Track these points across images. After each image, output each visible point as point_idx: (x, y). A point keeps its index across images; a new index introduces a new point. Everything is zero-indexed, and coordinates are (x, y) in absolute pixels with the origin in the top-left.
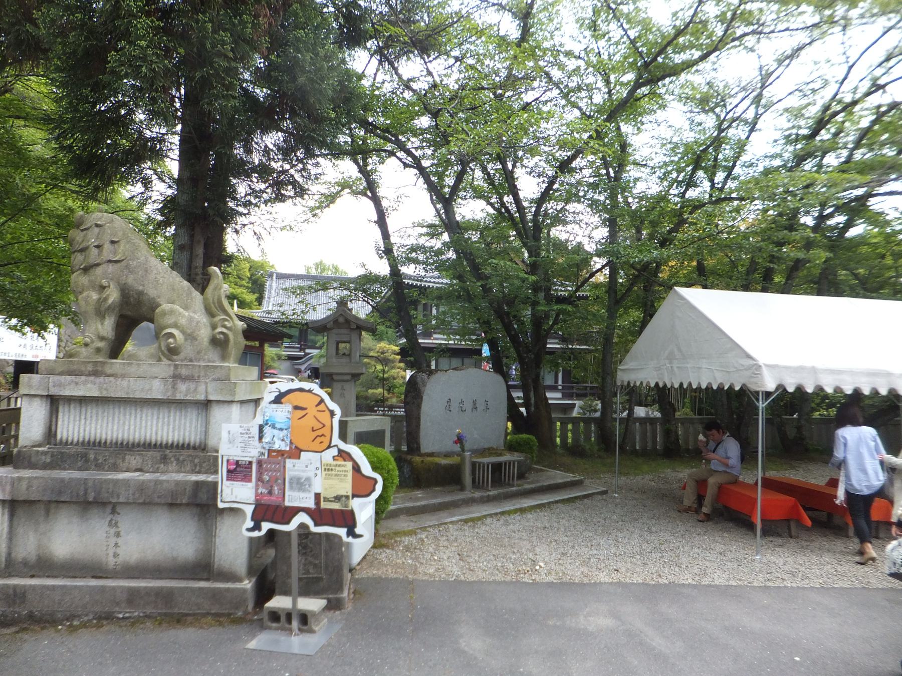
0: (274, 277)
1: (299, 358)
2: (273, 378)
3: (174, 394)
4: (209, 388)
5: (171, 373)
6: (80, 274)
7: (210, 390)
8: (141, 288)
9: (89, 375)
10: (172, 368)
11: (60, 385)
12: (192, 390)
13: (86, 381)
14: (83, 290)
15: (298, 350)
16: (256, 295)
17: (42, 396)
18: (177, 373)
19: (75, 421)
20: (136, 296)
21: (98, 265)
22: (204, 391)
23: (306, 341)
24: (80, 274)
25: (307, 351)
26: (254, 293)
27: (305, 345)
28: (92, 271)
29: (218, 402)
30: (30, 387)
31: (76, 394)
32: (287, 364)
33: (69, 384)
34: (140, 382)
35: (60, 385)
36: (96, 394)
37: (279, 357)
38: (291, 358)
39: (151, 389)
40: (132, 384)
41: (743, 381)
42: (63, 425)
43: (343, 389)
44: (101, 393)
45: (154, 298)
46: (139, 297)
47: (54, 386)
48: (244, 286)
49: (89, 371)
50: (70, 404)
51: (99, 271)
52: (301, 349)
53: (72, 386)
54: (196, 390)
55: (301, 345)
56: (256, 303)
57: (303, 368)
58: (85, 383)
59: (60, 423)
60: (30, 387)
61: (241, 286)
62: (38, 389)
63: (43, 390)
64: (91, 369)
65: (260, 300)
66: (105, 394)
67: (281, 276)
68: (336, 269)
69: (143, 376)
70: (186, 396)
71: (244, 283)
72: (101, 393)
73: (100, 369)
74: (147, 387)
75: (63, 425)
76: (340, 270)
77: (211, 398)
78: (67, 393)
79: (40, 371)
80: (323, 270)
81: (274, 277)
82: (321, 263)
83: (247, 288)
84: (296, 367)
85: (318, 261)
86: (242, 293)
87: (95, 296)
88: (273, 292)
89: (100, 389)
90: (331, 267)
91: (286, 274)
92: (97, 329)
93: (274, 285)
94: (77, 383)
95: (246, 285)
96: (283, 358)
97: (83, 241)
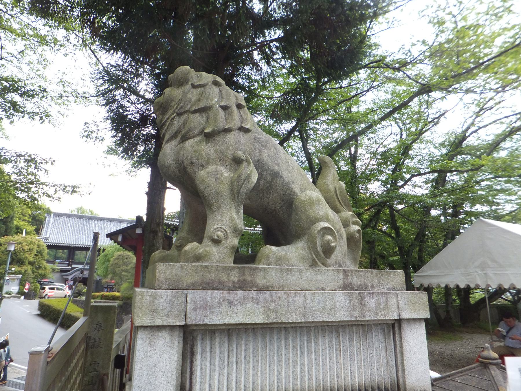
0: (52, 215)
1: (68, 271)
2: (50, 285)
3: (362, 314)
4: (400, 302)
5: (341, 283)
6: (200, 141)
7: (402, 305)
8: (276, 168)
9: (234, 288)
10: (341, 276)
11: (205, 307)
12: (383, 305)
13: (245, 298)
14: (208, 163)
15: (66, 265)
16: (35, 227)
17: (172, 328)
18: (348, 282)
19: (221, 369)
20: (269, 178)
21: (228, 131)
22: (395, 307)
23: (73, 259)
24: (200, 141)
25: (73, 266)
26: (33, 226)
27: (72, 262)
28: (220, 138)
29: (408, 320)
30: (154, 311)
31: (232, 321)
32: (58, 275)
33: (220, 304)
34: (319, 297)
35: (205, 307)
36: (260, 319)
37: (54, 270)
38: (62, 271)
39: (333, 308)
40: (309, 301)
41: (428, 283)
42: (203, 377)
43: (397, 295)
44: (268, 317)
45: (288, 183)
46: (273, 179)
47: (195, 309)
48: (26, 220)
49: (234, 283)
50: (212, 339)
51: (231, 138)
52: (69, 265)
53: (224, 307)
54: (386, 305)
55: (69, 262)
56: (34, 233)
57: (70, 278)
58: (243, 301)
59: (198, 373)
60: (154, 311)
61: (23, 220)
62: (167, 316)
63: (178, 316)
64: (236, 279)
65: (38, 231)
66: (273, 318)
67: (56, 215)
68: (92, 212)
69: (307, 287)
70: (377, 314)
71: (26, 218)
72: (268, 317)
73: (249, 278)
74: (329, 304)
75: (203, 377)
76: (94, 213)
77: (405, 315)
78: (216, 319)
79: (157, 283)
80: (83, 212)
81: (52, 215)
82: (81, 208)
83: (29, 222)
84: (65, 277)
85: (79, 207)
86: (25, 225)
87: (226, 173)
88: (50, 225)
89: (267, 310)
90: (88, 211)
91: (61, 213)
92: (231, 218)
93: (52, 220)
94: (231, 303)
95: (27, 219)
96: (57, 271)
97: (199, 100)
